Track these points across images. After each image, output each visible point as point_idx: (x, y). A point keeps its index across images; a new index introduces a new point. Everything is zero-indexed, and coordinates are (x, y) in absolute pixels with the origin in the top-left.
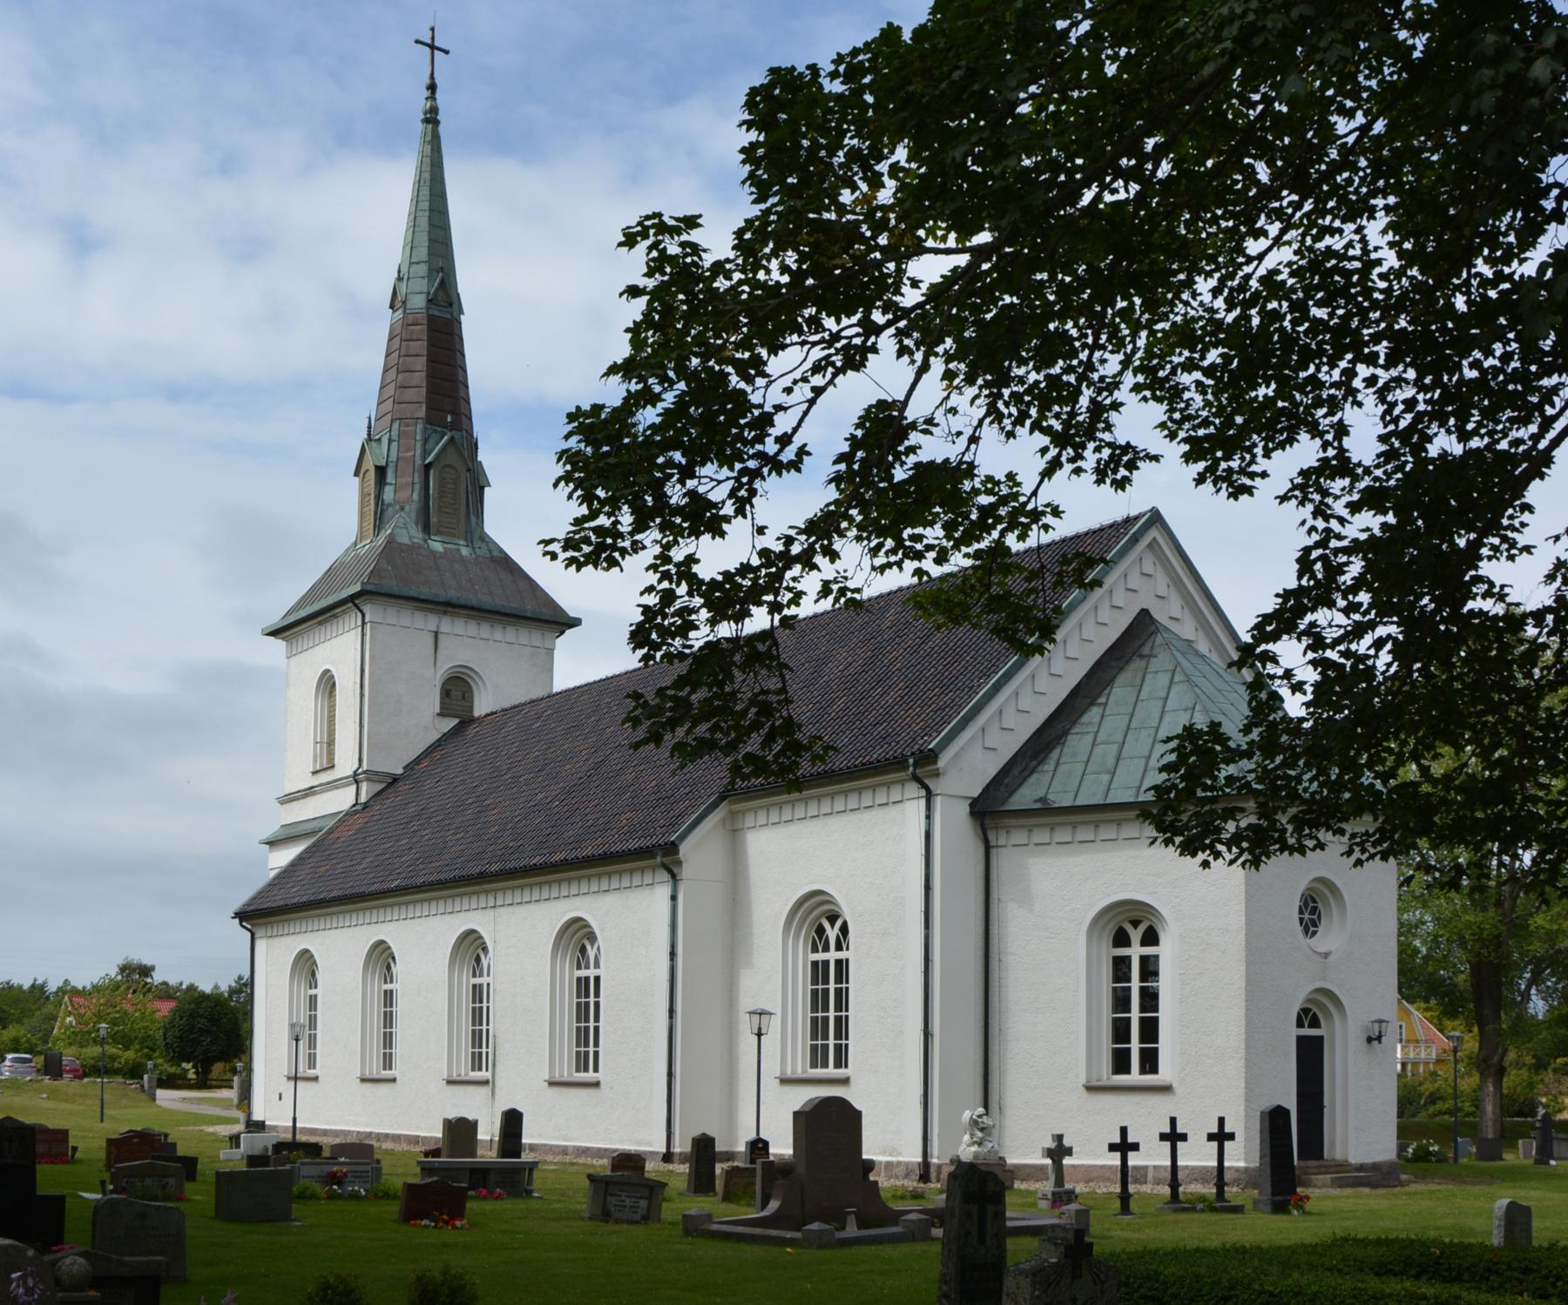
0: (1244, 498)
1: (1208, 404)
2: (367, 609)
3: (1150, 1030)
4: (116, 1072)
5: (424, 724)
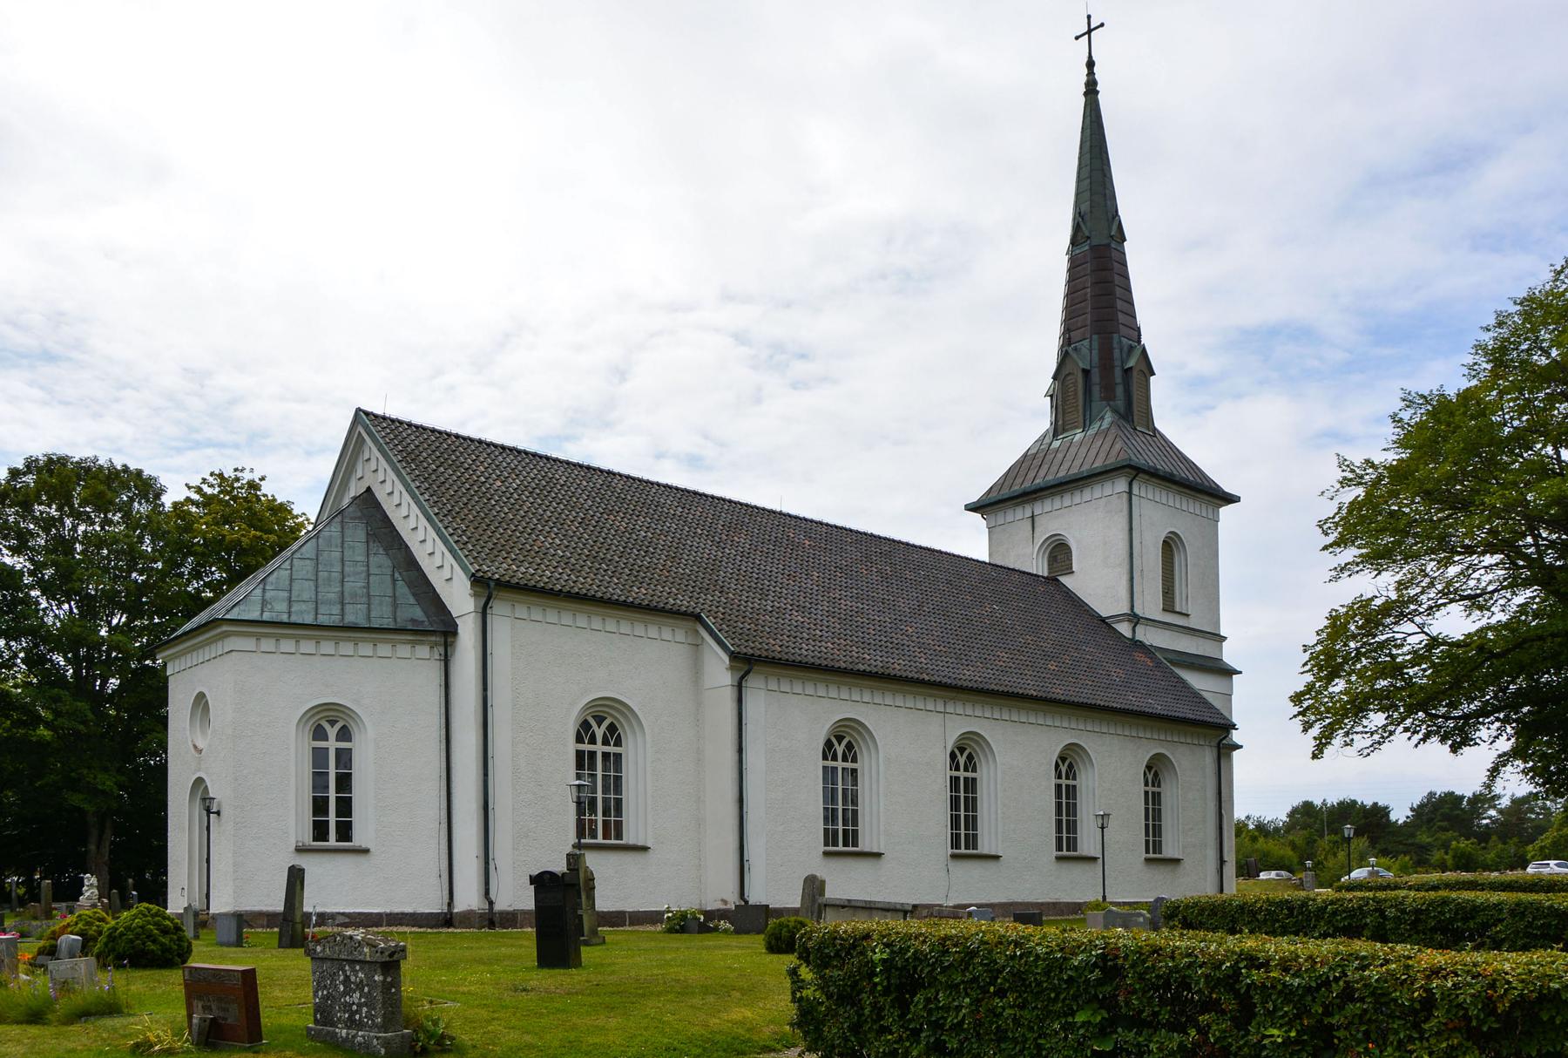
3: (345, 807)
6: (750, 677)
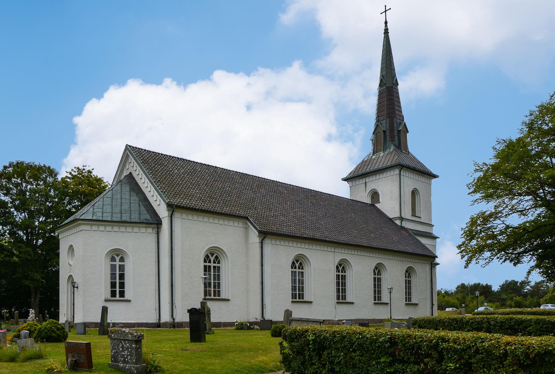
3: (122, 285)
6: (266, 239)
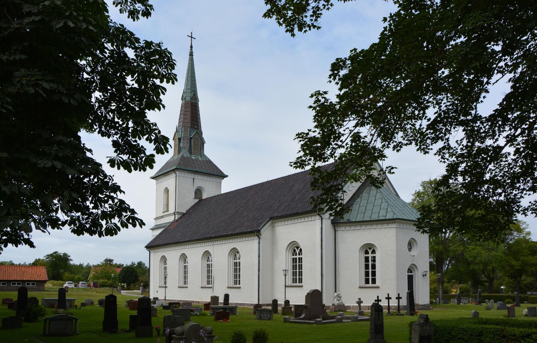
0: (427, 154)
1: (411, 132)
2: (177, 173)
3: (374, 274)
4: (107, 286)
5: (190, 201)
